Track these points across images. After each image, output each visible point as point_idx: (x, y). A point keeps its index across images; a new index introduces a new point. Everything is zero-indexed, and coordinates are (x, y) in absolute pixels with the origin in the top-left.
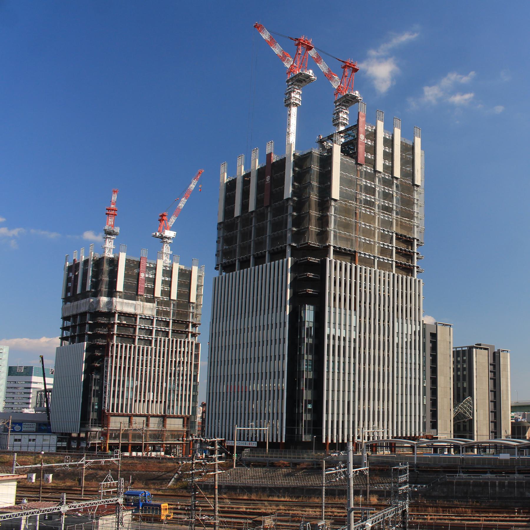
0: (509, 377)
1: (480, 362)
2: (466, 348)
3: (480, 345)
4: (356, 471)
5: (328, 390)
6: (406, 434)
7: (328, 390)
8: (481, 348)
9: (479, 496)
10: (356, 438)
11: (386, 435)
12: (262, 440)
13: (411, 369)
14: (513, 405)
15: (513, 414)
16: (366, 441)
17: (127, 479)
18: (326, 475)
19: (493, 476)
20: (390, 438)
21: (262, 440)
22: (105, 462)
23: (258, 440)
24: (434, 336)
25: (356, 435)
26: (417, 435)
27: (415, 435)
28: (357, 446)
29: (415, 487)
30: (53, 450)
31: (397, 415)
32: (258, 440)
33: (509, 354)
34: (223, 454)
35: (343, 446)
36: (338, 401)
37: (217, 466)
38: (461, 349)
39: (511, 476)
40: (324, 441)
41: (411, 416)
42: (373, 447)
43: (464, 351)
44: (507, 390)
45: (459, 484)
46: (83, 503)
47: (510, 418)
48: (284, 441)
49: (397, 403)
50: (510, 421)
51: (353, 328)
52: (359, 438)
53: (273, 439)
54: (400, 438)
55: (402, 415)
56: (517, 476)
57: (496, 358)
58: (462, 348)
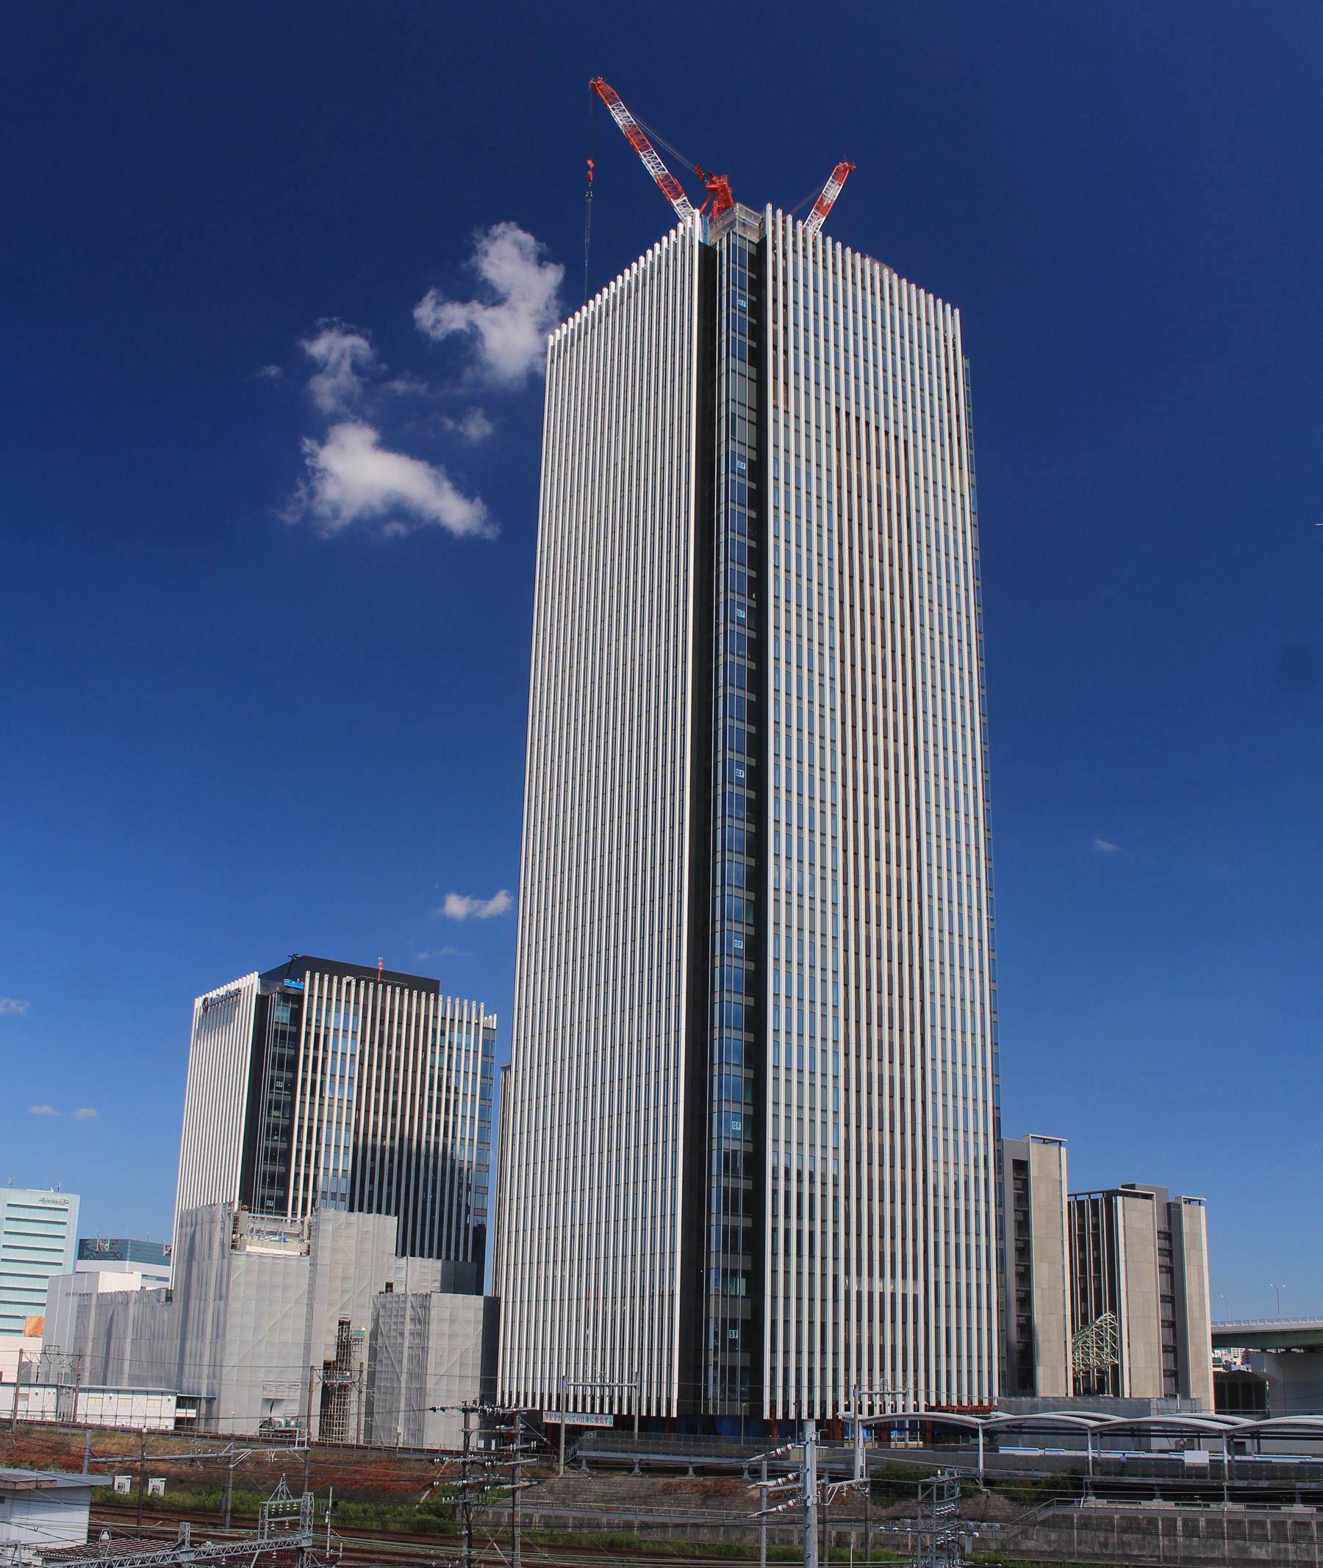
0: (1205, 1264)
1: (1136, 1226)
3: (1132, 1186)
5: (774, 1297)
6: (960, 1402)
7: (774, 1297)
8: (1136, 1195)
9: (1136, 1552)
10: (842, 1408)
11: (911, 1402)
12: (625, 1412)
14: (1216, 1331)
15: (1218, 1352)
16: (865, 1415)
17: (321, 1495)
19: (1170, 1505)
20: (922, 1411)
21: (625, 1412)
23: (616, 1411)
24: (1021, 1167)
25: (842, 1402)
27: (981, 1402)
28: (833, 1431)
30: (170, 1425)
31: (938, 1356)
32: (616, 1411)
33: (1202, 1208)
34: (534, 1444)
35: (792, 1429)
39: (1214, 1506)
40: (767, 1415)
41: (980, 1357)
42: (881, 1431)
44: (1202, 1295)
45: (1086, 1524)
46: (229, 1545)
47: (1210, 1363)
48: (674, 1415)
49: (937, 1328)
50: (1211, 1370)
52: (847, 1408)
53: (649, 1410)
54: (949, 1409)
55: (823, 1352)
56: (1228, 1506)
57: (1172, 1215)
58: (1089, 1194)
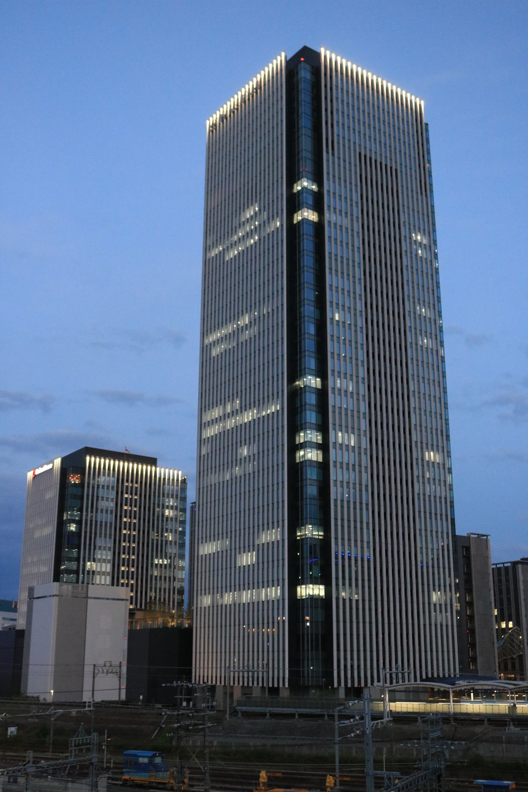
2: (509, 564)
4: (378, 723)
13: (355, 521)
18: (340, 728)
22: (78, 712)
26: (452, 676)
29: (452, 744)
36: (358, 623)
37: (206, 718)
38: (502, 565)
43: (507, 568)
51: (356, 249)
58: (504, 563)
